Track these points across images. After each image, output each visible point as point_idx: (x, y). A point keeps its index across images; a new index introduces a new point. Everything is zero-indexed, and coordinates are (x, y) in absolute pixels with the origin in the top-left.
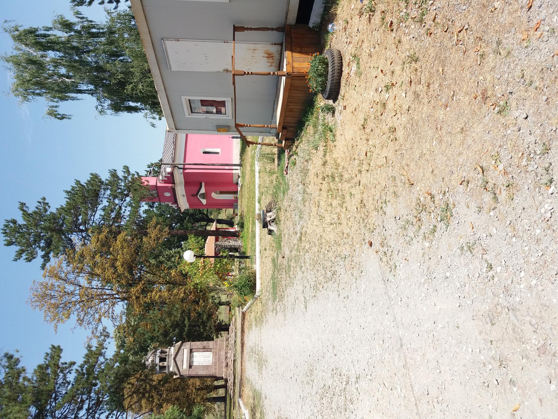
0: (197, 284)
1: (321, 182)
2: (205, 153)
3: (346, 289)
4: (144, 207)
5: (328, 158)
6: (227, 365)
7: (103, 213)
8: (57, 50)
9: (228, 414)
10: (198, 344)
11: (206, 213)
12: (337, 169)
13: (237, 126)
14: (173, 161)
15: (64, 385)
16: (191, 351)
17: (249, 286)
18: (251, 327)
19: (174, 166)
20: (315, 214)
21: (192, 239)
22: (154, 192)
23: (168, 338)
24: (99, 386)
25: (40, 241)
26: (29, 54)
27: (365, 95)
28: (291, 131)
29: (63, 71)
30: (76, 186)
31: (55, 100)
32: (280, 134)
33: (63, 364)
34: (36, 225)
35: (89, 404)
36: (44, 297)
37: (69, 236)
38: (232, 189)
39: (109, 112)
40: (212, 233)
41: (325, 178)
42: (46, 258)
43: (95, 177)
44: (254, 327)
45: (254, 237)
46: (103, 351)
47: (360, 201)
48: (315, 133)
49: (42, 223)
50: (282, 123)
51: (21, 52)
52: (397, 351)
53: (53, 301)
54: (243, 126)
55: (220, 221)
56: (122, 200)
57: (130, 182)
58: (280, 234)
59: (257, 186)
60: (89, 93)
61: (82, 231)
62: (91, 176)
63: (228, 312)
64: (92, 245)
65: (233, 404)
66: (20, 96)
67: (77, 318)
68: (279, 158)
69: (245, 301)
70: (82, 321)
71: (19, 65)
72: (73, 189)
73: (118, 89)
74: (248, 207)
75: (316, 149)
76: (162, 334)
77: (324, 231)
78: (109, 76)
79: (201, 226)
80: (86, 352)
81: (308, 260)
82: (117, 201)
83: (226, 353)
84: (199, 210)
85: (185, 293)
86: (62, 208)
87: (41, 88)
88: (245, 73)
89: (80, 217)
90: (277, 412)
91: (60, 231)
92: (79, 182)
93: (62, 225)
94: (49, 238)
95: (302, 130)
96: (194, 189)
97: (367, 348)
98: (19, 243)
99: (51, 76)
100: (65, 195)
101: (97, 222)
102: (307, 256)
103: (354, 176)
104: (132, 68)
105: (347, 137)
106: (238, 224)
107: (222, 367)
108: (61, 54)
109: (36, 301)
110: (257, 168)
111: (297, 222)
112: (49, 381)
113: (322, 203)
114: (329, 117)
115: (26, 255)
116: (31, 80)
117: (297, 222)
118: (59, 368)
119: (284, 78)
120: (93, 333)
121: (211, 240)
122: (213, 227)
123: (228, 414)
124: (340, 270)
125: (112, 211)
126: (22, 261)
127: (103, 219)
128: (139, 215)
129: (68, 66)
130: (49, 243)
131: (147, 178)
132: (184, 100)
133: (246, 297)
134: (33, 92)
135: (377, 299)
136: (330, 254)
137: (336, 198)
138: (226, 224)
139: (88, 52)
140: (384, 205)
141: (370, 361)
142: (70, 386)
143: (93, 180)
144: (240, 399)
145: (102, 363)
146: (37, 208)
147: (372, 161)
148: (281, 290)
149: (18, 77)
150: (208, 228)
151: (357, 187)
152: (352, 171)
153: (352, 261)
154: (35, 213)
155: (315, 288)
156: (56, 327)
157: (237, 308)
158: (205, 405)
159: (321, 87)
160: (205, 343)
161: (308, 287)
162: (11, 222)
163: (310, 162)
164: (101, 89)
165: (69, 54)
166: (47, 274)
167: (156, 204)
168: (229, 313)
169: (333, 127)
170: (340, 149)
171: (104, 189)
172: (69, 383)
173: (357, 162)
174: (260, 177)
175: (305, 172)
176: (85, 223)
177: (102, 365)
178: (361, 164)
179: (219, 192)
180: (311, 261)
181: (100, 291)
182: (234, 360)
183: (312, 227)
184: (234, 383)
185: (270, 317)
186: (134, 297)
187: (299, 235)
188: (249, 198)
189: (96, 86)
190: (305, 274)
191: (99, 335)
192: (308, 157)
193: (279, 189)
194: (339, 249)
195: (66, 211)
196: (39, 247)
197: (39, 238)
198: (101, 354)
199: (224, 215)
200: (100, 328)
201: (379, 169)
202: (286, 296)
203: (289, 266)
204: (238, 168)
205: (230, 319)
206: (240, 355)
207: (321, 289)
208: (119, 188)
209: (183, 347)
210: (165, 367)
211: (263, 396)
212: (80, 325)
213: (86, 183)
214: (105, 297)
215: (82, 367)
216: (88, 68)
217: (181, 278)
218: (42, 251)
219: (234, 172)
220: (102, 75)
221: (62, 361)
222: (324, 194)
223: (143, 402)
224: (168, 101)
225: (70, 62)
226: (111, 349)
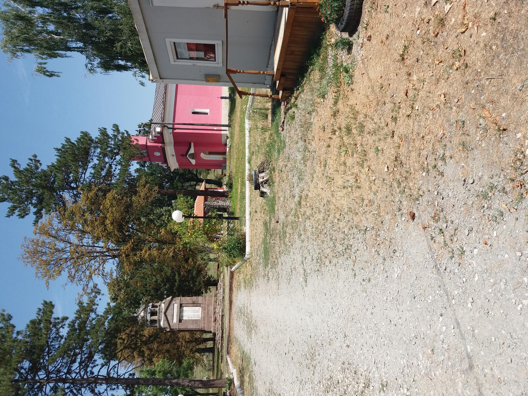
0: (186, 243)
1: (330, 135)
2: (194, 113)
3: (367, 270)
4: (134, 166)
5: (340, 105)
6: (215, 320)
7: (93, 171)
8: (46, 7)
9: (216, 365)
10: (188, 299)
11: (195, 173)
12: (355, 119)
13: (229, 72)
14: (163, 121)
15: (57, 340)
16: (181, 306)
17: (238, 248)
18: (240, 288)
19: (163, 126)
20: (320, 175)
21: (181, 199)
22: (144, 151)
23: (159, 292)
24: (90, 341)
25: (32, 198)
26: (17, 10)
27: (405, 15)
28: (290, 80)
29: (51, 27)
30: (66, 143)
31: (44, 57)
32: (278, 82)
33: (55, 319)
34: (28, 182)
35: (81, 359)
36: (35, 253)
37: (61, 193)
38: (221, 150)
39: (99, 70)
40: (201, 193)
41: (335, 131)
42: (38, 215)
43: (85, 135)
44: (242, 288)
45: (244, 198)
46: (94, 307)
47: (393, 158)
48: (321, 78)
49: (34, 180)
50: (281, 69)
51: (10, 8)
52: (463, 372)
53: (44, 258)
54: (235, 72)
55: (208, 182)
56: (112, 159)
57: (120, 141)
58: (274, 197)
59: (247, 145)
60: (78, 51)
61: (73, 189)
62: (82, 134)
63: (217, 268)
64: (82, 202)
65: (220, 358)
66: (9, 53)
67: (68, 275)
68: (274, 113)
69: (235, 262)
70: (74, 278)
71: (8, 21)
72: (63, 147)
73: (107, 47)
74: (236, 167)
75: (323, 97)
76: (153, 289)
77: (333, 195)
78: (98, 34)
79: (191, 186)
80: (77, 308)
81: (310, 229)
82: (107, 160)
83: (215, 308)
84: (189, 170)
85: (174, 252)
86: (53, 166)
87: (30, 45)
88: (240, 2)
89: (71, 175)
90: (268, 384)
91: (52, 189)
92: (69, 139)
93: (54, 182)
94: (40, 195)
95: (303, 77)
96: (183, 149)
97: (401, 352)
98: (11, 200)
99: (40, 33)
100: (56, 152)
101: (88, 180)
102: (308, 223)
103: (383, 125)
104: (121, 25)
105: (372, 76)
106: (226, 185)
107: (210, 322)
108: (50, 11)
109: (27, 258)
110: (247, 124)
111: (295, 184)
112: (41, 336)
113: (330, 162)
114: (343, 55)
115: (19, 211)
116: (19, 36)
117: (295, 184)
118: (51, 323)
119: (286, 10)
120: (84, 290)
121: (200, 200)
122: (202, 187)
123: (216, 365)
124: (357, 244)
125: (102, 170)
126: (15, 217)
127: (93, 177)
128: (130, 174)
129: (56, 22)
130: (41, 200)
131: (137, 138)
132: (169, 42)
133: (236, 259)
134: (22, 49)
135: (421, 291)
136: (342, 224)
137: (353, 155)
138: (215, 184)
139: (77, 8)
140: (440, 163)
141: (406, 371)
142: (63, 340)
143: (83, 138)
144: (228, 356)
145: (93, 319)
146: (28, 165)
147: (418, 103)
148: (274, 256)
149: (6, 33)
150: (197, 188)
151: (389, 140)
152: (380, 119)
153: (377, 235)
154: (26, 170)
155: (320, 261)
156: (47, 283)
157: (225, 268)
158: (193, 357)
159: (337, 15)
160: (194, 298)
161: (309, 258)
162: (3, 178)
163: (314, 114)
164: (90, 47)
165: (57, 10)
166: (38, 231)
167: (147, 164)
168: (218, 270)
169: (350, 66)
170: (360, 93)
171: (94, 147)
172: (62, 337)
173: (389, 106)
174: (250, 136)
175: (307, 126)
176: (76, 180)
177: (94, 321)
178: (397, 107)
179: (207, 152)
180: (314, 229)
181: (90, 248)
182: (223, 316)
183: (316, 189)
184: (222, 337)
185: (261, 281)
186: (124, 256)
187: (297, 199)
188: (238, 159)
189: (85, 43)
190: (305, 243)
191: (90, 291)
192: (310, 109)
193: (273, 147)
194: (356, 219)
195: (56, 168)
196: (32, 203)
197: (31, 195)
198: (92, 311)
199: (211, 176)
200: (91, 285)
201: (431, 113)
202: (280, 264)
203: (285, 233)
204: (227, 128)
205: (219, 276)
206: (228, 312)
207: (327, 263)
208: (108, 147)
209: (173, 302)
210: (156, 321)
211: (252, 361)
212: (72, 281)
213: (76, 141)
214: (95, 254)
215: (73, 322)
216: (77, 24)
217: (170, 237)
218: (34, 207)
219: (223, 132)
220: (90, 32)
221: (54, 316)
222: (334, 150)
223: (135, 353)
224: (151, 45)
225: (59, 19)
226: (104, 303)
